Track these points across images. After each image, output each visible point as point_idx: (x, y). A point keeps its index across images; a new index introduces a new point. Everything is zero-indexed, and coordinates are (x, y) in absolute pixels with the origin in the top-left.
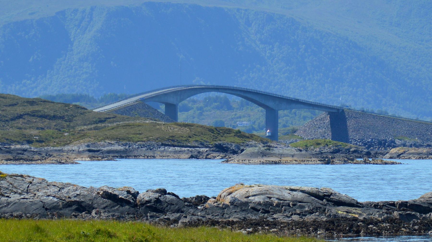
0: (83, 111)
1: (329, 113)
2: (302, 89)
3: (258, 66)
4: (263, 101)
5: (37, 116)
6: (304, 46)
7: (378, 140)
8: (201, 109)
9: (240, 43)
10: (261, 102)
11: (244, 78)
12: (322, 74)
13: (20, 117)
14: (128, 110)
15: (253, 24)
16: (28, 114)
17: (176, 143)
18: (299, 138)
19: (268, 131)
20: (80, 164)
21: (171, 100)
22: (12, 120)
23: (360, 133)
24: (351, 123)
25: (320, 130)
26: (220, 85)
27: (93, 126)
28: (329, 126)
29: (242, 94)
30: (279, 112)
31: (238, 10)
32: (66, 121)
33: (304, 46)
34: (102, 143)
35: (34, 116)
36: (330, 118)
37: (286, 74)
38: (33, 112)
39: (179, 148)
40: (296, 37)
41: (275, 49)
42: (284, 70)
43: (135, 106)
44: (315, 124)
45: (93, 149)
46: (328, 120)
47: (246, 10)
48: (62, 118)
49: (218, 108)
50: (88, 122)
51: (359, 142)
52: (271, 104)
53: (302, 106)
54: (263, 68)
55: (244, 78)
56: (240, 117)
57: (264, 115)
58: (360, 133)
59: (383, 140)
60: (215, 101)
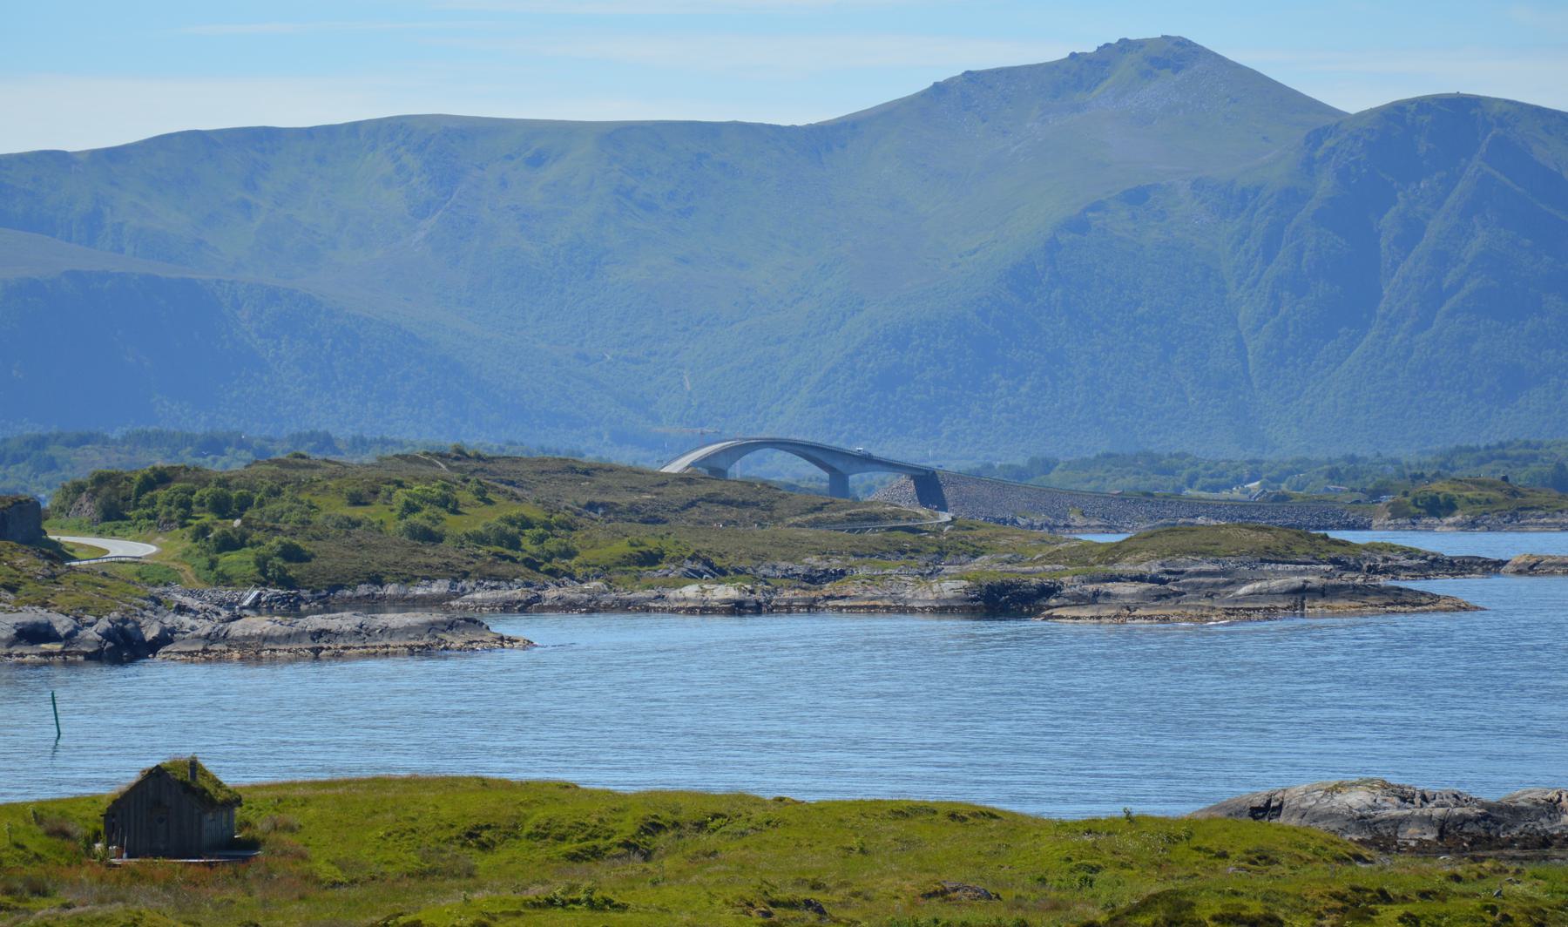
1: (912, 477)
2: (330, 411)
3: (256, 374)
4: (829, 462)
5: (717, 502)
6: (330, 340)
9: (226, 336)
11: (235, 394)
12: (361, 387)
13: (692, 504)
15: (245, 305)
16: (702, 499)
17: (1279, 558)
20: (1476, 608)
22: (684, 509)
27: (810, 517)
28: (916, 498)
29: (802, 450)
30: (851, 478)
31: (219, 282)
32: (763, 510)
33: (330, 340)
34: (1183, 560)
35: (711, 502)
37: (303, 388)
38: (709, 495)
39: (1293, 566)
40: (316, 325)
41: (283, 346)
42: (299, 380)
45: (1174, 569)
47: (232, 282)
48: (756, 504)
50: (799, 511)
52: (839, 465)
54: (265, 378)
55: (235, 394)
57: (798, 481)
60: (310, 440)
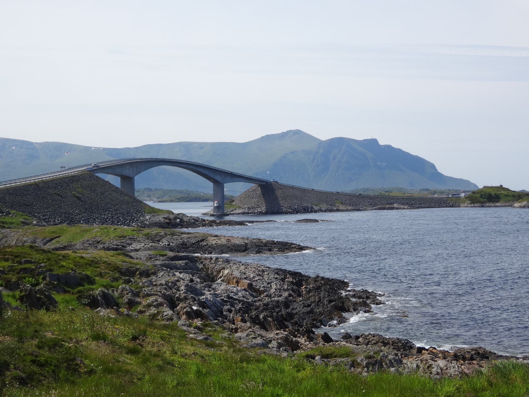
0: (160, 200)
1: (260, 185)
4: (211, 175)
7: (303, 207)
8: (143, 191)
10: (210, 176)
14: (67, 182)
18: (237, 207)
19: (216, 202)
21: (127, 172)
23: (288, 201)
24: (279, 193)
25: (254, 200)
26: (174, 159)
29: (194, 168)
36: (261, 189)
43: (79, 177)
44: (248, 195)
46: (259, 191)
49: (148, 191)
51: (289, 209)
52: (218, 178)
53: (241, 179)
56: (155, 194)
58: (288, 201)
59: (306, 207)
